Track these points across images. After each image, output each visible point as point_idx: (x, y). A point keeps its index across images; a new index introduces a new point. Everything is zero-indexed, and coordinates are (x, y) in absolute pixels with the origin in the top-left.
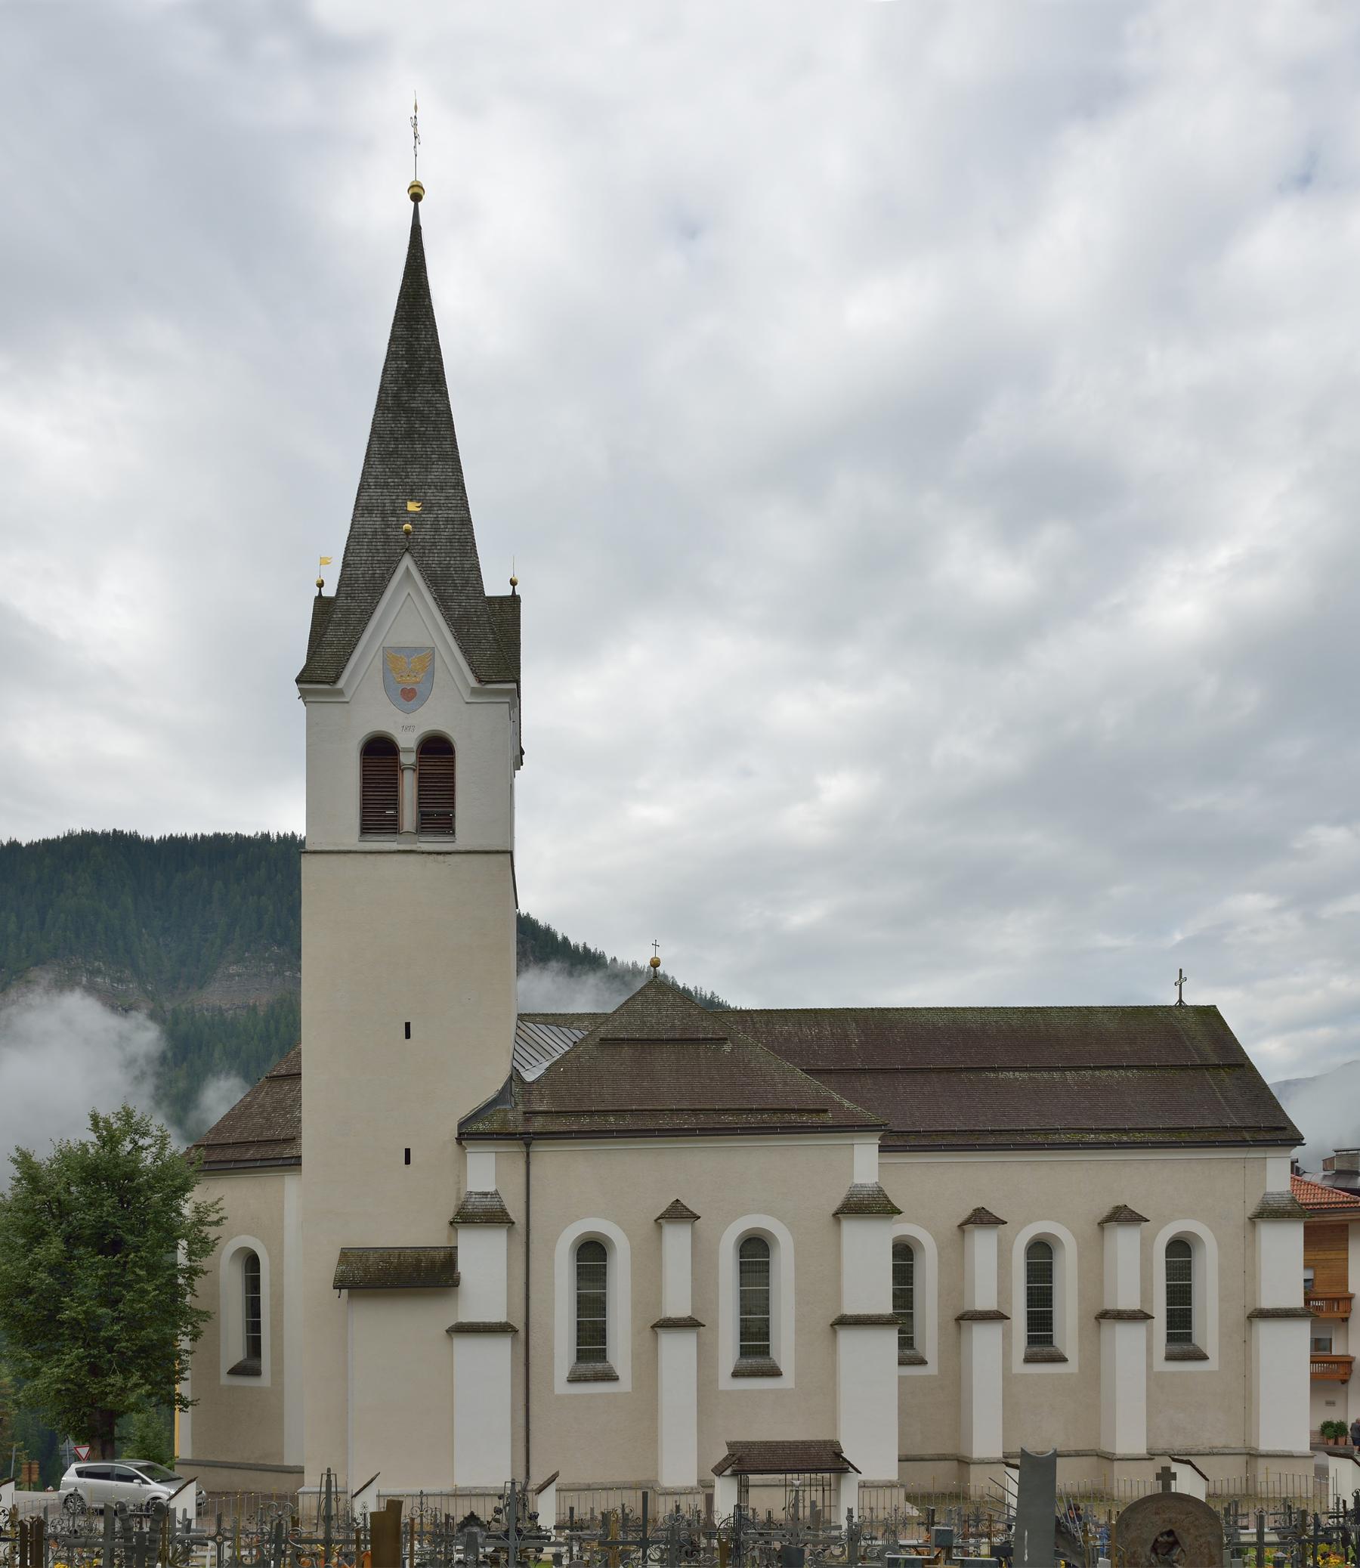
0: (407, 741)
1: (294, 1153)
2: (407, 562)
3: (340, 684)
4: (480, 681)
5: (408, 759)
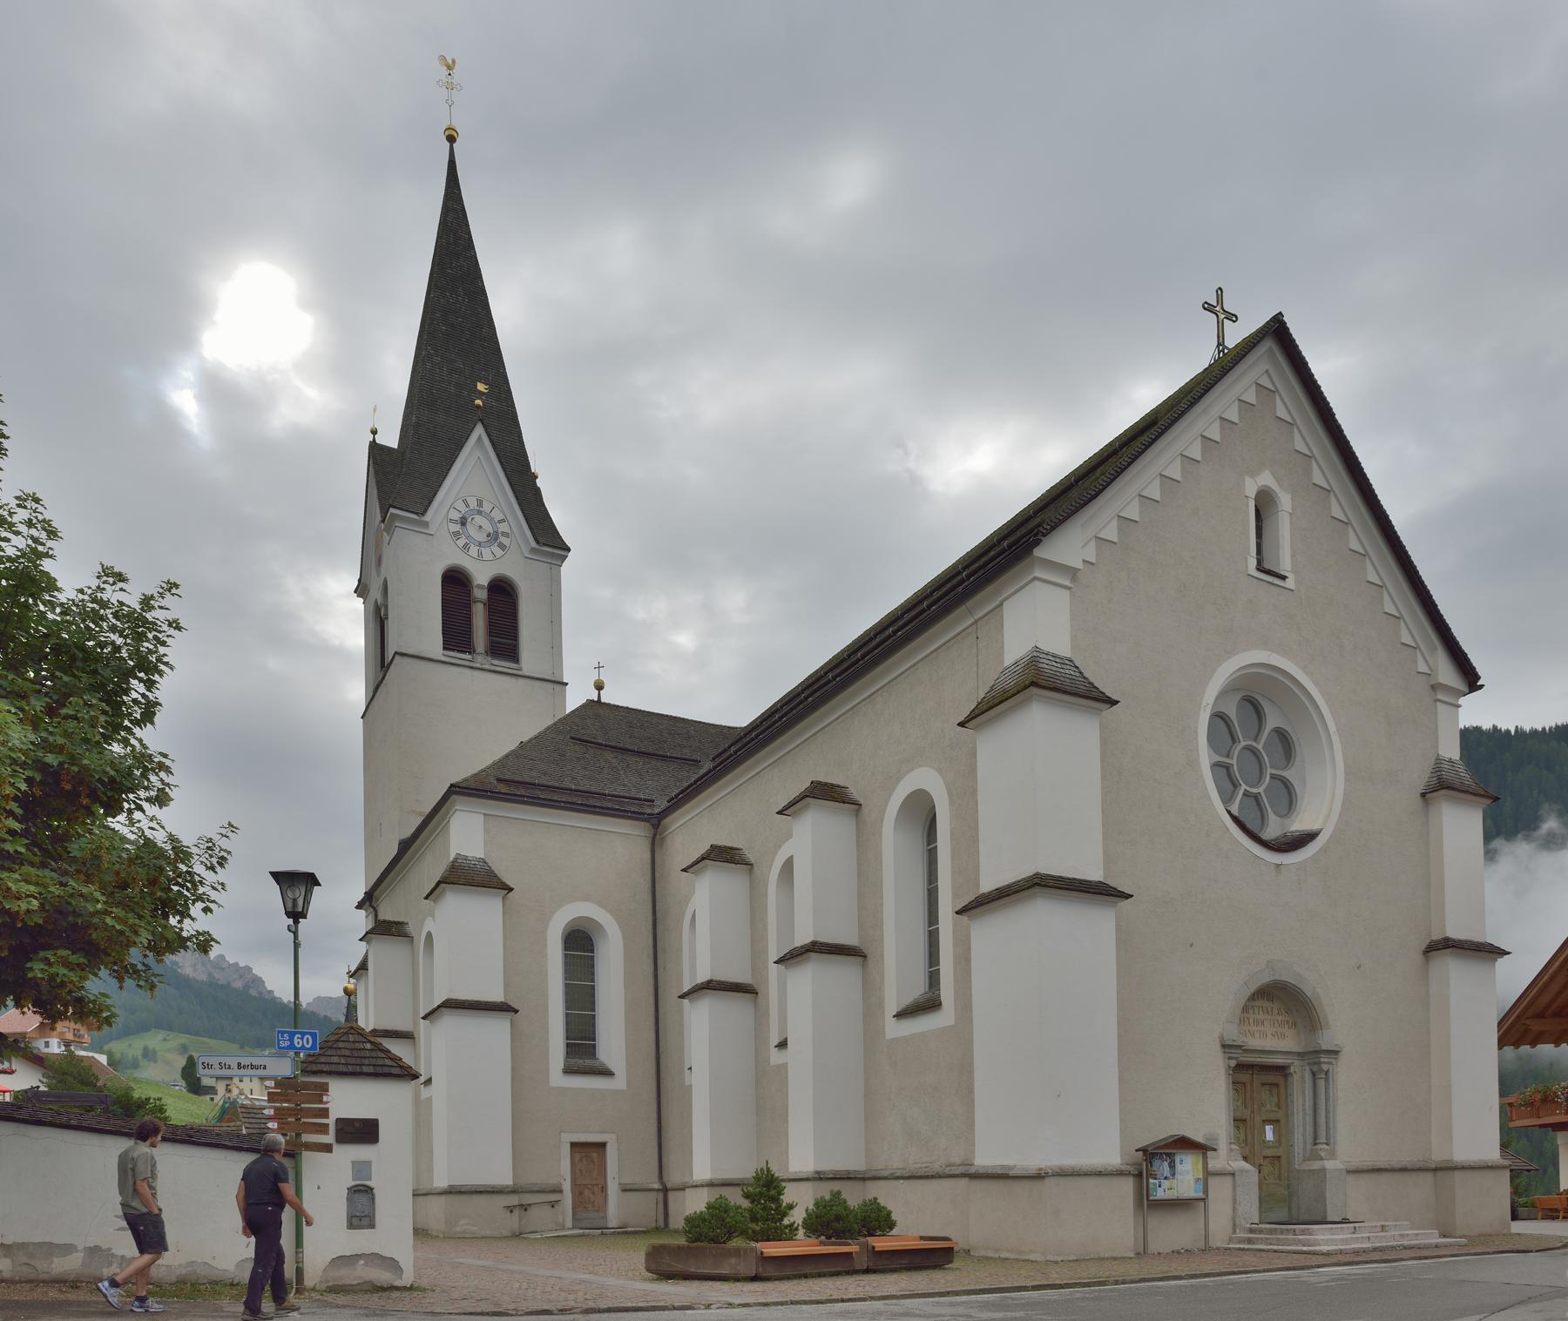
0: (481, 576)
1: (1509, 1051)
2: (479, 431)
3: (428, 517)
4: (538, 542)
5: (481, 594)
